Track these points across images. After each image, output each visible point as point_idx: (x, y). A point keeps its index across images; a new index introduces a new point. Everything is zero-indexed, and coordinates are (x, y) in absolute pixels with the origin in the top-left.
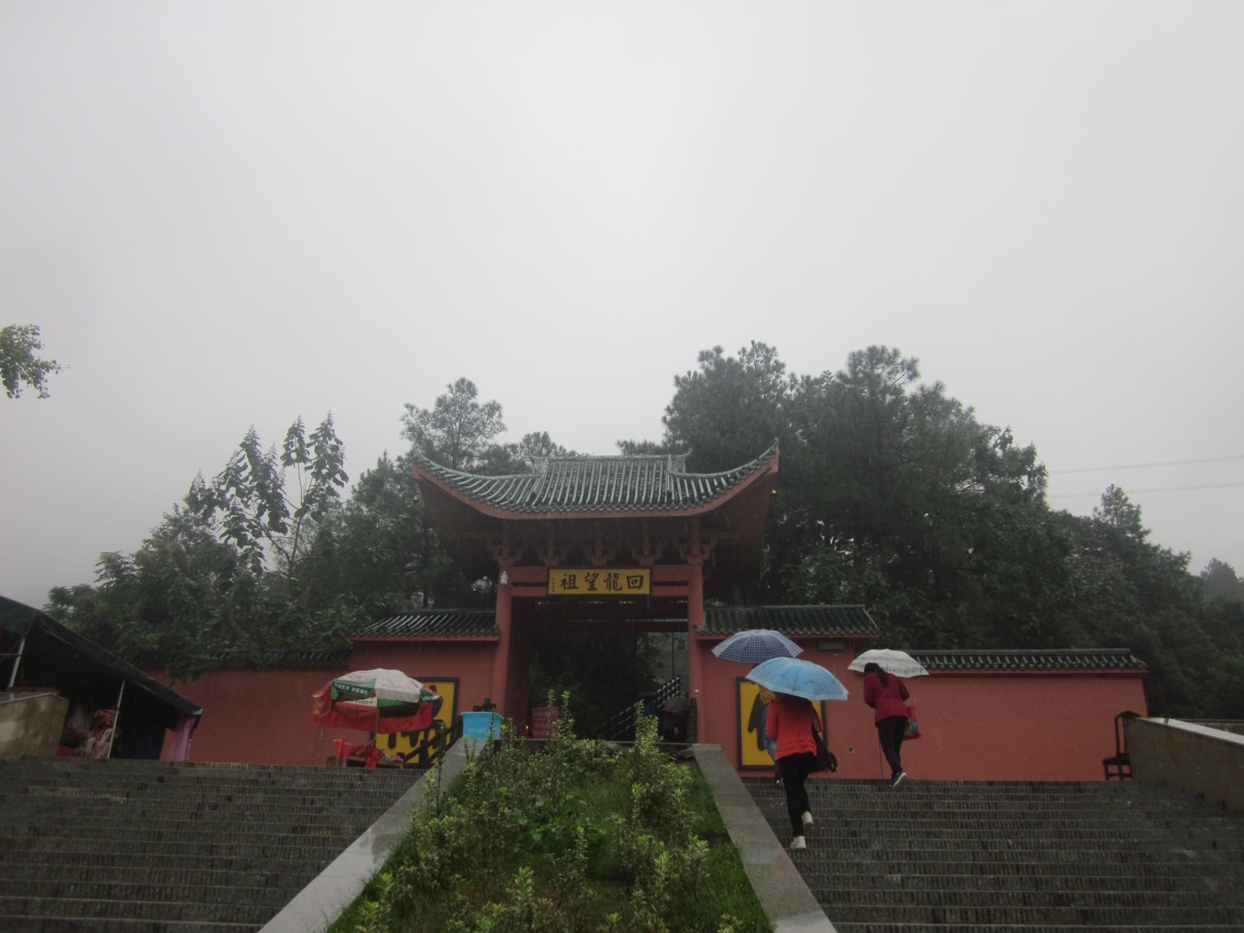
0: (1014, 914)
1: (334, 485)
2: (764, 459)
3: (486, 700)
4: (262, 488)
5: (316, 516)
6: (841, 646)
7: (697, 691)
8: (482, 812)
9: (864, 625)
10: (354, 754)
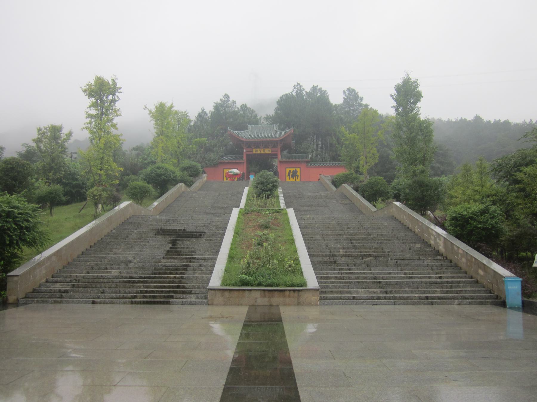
6: (303, 162)
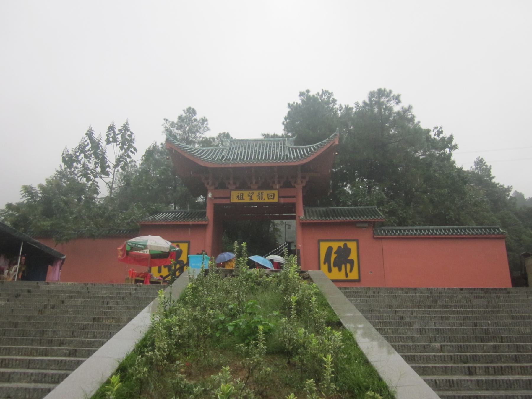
0: (517, 370)
1: (130, 153)
2: (332, 138)
4: (95, 153)
5: (123, 168)
6: (366, 225)
8: (196, 313)
9: (377, 215)
10: (138, 276)
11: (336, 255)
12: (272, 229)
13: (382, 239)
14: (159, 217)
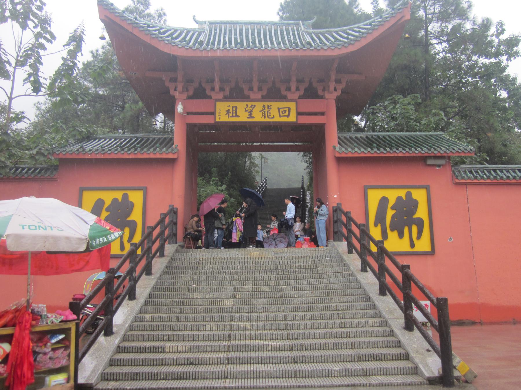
3: (169, 206)
6: (442, 162)
7: (335, 196)
9: (370, 147)
11: (394, 212)
12: (247, 164)
13: (466, 184)
14: (91, 146)
